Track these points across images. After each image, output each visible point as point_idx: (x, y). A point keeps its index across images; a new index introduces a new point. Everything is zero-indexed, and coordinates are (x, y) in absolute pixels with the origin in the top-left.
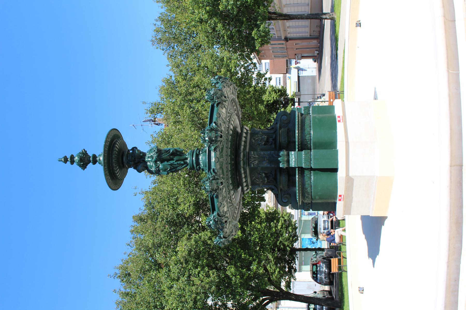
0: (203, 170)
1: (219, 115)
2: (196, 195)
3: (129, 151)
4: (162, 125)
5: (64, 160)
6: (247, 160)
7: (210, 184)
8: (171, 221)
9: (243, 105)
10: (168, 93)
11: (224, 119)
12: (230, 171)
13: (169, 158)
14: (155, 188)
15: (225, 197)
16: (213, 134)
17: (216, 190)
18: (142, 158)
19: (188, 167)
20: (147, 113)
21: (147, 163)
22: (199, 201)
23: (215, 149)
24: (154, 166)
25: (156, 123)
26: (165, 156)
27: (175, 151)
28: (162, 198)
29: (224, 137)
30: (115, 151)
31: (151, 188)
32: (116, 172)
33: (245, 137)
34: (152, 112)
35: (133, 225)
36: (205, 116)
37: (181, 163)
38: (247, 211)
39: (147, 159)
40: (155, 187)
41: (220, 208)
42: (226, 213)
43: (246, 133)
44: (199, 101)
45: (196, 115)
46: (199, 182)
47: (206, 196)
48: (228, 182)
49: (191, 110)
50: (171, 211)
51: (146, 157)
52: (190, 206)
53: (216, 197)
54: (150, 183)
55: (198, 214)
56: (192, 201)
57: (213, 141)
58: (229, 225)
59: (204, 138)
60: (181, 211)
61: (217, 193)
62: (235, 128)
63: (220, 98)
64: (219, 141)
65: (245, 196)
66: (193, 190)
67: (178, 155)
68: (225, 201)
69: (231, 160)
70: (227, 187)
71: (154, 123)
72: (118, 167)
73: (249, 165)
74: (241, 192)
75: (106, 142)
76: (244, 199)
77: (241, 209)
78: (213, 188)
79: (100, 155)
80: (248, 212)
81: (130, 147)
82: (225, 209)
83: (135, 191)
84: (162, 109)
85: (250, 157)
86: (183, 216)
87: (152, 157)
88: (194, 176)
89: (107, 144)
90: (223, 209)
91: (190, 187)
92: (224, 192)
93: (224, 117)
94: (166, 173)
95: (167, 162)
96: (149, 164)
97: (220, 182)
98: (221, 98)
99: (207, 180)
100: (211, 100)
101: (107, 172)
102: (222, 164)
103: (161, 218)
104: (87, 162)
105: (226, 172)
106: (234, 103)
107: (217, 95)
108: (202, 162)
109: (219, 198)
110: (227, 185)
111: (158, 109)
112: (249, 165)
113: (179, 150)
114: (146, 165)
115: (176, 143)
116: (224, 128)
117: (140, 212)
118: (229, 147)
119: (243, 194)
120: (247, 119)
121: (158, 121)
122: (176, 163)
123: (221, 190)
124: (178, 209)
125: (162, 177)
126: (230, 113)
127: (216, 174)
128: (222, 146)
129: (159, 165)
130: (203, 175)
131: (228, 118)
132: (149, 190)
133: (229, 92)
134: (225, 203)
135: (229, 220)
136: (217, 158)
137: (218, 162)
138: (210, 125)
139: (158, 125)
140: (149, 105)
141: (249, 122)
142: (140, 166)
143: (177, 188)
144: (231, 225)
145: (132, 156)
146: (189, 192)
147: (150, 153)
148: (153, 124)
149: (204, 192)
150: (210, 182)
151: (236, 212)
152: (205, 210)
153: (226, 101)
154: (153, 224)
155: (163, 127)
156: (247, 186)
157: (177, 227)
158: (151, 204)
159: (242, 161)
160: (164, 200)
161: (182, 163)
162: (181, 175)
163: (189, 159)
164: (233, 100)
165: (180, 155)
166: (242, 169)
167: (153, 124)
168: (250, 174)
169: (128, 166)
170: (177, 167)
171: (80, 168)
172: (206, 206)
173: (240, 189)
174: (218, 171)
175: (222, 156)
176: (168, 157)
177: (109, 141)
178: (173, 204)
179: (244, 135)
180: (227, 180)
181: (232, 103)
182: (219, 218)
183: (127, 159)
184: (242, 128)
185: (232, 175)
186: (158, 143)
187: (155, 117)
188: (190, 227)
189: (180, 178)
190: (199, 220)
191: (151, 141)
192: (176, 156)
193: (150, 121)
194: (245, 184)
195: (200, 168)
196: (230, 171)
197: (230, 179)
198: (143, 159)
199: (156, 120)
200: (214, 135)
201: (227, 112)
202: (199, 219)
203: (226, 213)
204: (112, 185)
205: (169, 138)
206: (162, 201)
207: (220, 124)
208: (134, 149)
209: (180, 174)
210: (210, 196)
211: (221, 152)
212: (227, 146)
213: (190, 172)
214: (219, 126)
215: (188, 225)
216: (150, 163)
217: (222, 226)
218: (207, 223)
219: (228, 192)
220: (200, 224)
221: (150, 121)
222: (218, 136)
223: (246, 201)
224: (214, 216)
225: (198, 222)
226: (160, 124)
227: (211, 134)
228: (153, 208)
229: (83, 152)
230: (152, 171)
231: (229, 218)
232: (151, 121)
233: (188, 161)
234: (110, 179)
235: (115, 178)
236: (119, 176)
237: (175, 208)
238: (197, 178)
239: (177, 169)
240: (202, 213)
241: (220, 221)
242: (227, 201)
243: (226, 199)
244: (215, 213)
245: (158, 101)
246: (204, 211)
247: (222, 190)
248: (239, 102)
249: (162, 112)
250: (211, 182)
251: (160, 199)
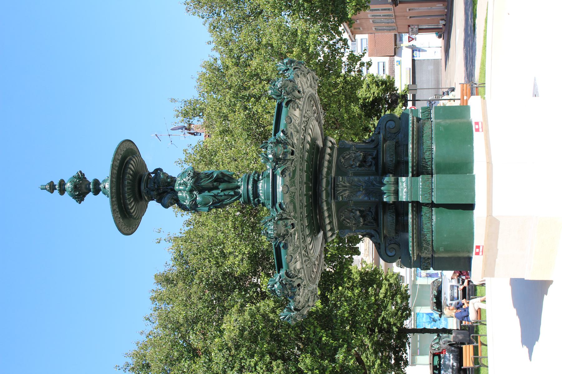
32: (130, 207)
105: (300, 209)
181: (309, 101)
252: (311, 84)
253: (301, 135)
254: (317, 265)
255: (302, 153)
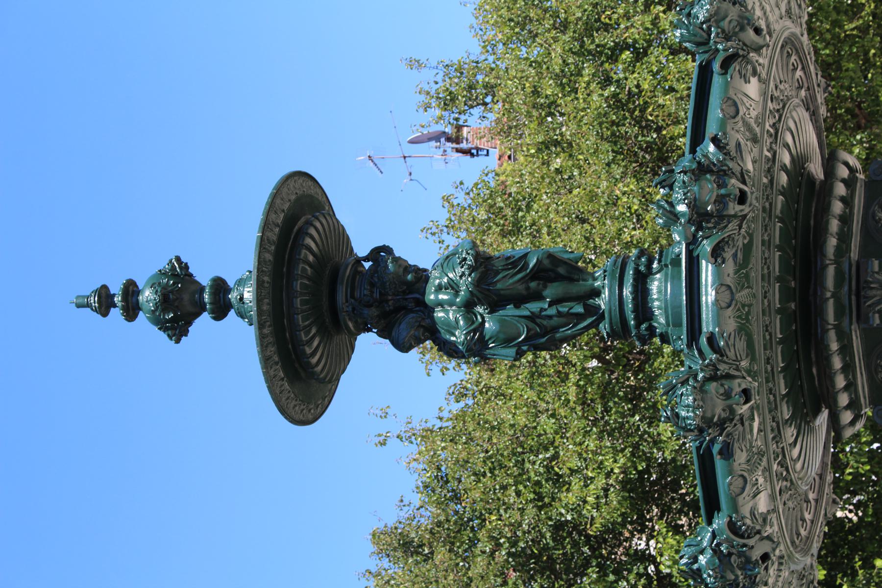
0: (665, 339)
1: (733, 108)
2: (636, 447)
3: (358, 261)
4: (487, 155)
5: (99, 302)
6: (853, 298)
7: (695, 400)
8: (529, 552)
9: (829, 65)
10: (511, 20)
11: (754, 126)
12: (781, 341)
13: (524, 292)
14: (461, 417)
15: (761, 454)
16: (708, 190)
17: (721, 425)
18: (411, 292)
19: (604, 328)
20: (427, 107)
21: (432, 310)
22: (647, 471)
23: (717, 253)
24: (461, 323)
25: (464, 145)
26: (506, 283)
27: (546, 262)
28: (490, 457)
29: (754, 202)
30: (301, 265)
31: (445, 414)
32: (308, 351)
33: (843, 199)
34: (449, 101)
35: (373, 571)
36: (670, 115)
37: (572, 311)
38: (850, 516)
39: (432, 297)
40: (462, 411)
41: (740, 498)
42: (765, 520)
43: (850, 183)
44: (640, 55)
45: (632, 112)
46: (644, 389)
47: (676, 451)
48: (771, 390)
49: (606, 94)
50: (531, 511)
51: (429, 285)
52: (606, 490)
53: (720, 453)
54: (444, 394)
55: (642, 526)
56: (616, 471)
57: (707, 216)
58: (780, 570)
59: (671, 205)
60: (572, 510)
61: (728, 435)
62: (800, 162)
63: (735, 34)
64: (735, 216)
65: (843, 450)
66: (622, 425)
67: (558, 278)
68: (761, 468)
69: (786, 295)
70: (770, 412)
71: (455, 145)
72: (314, 331)
73: (862, 317)
74: (828, 433)
75: (266, 226)
76: (838, 465)
77: (827, 504)
78: (709, 415)
79: (241, 282)
80: (855, 519)
81: (361, 248)
82: (763, 504)
83: (383, 427)
84: (490, 89)
85: (867, 282)
86: (580, 533)
87: (453, 287)
88: (624, 366)
89: (269, 234)
90: (751, 504)
91: (607, 410)
92: (755, 430)
93: (754, 114)
94: (512, 352)
95: (517, 307)
96: (441, 314)
97: (737, 389)
98: (742, 35)
99: (684, 383)
100: (698, 44)
101: (272, 349)
102: (748, 313)
103: (491, 538)
104: (191, 309)
105: (765, 349)
106: (793, 58)
107: (722, 24)
108: (659, 308)
109: (736, 457)
110: (769, 402)
111: (471, 87)
112: (862, 317)
113: (566, 256)
114: (428, 321)
115: (549, 227)
116: (754, 162)
117: (404, 514)
118: (777, 241)
119: (838, 439)
120: (845, 123)
121: (470, 139)
122: (552, 311)
123: (743, 424)
124: (557, 504)
125: (492, 370)
126: (777, 98)
127: (722, 355)
128: (744, 237)
129: (484, 321)
130: (661, 363)
131: (772, 121)
132: (439, 424)
133: (772, 10)
134: (761, 480)
135: (777, 552)
136: (723, 288)
137: (729, 306)
138: (693, 151)
139: (472, 155)
140: (436, 71)
141: (858, 137)
142: (403, 326)
143: (553, 416)
144: (785, 574)
145: (372, 285)
146: (602, 432)
147: (446, 270)
148: (449, 150)
149: (665, 429)
150: (695, 388)
151: (808, 516)
152: (670, 510)
153: (762, 47)
154: (458, 564)
155: (492, 162)
156: (854, 405)
157: (556, 579)
158: (447, 482)
159: (831, 301)
160: (501, 466)
161: (579, 309)
162: (568, 362)
163: (606, 294)
164: (791, 44)
165: (570, 279)
166: (832, 335)
167: (449, 150)
168: (868, 354)
169: (356, 324)
170: (555, 329)
171: (163, 336)
172: (676, 492)
173: (823, 418)
174: (731, 342)
175: (744, 280)
176: (521, 288)
177: (279, 222)
178: (538, 483)
179: (840, 189)
180: (767, 381)
181: (785, 55)
182: (738, 541)
183: (352, 296)
184: (830, 162)
185: (790, 358)
186: (473, 229)
187: (461, 123)
188: (612, 577)
189: (567, 375)
190: (648, 549)
191: (443, 222)
192: (552, 280)
193: (437, 137)
194: (844, 400)
195: (652, 330)
196: (779, 343)
197: (781, 376)
198: (417, 296)
199: (465, 135)
200: (712, 191)
201: (764, 94)
202: (647, 545)
203: (765, 520)
204: (294, 403)
205: (520, 209)
206: (492, 470)
207: (738, 145)
208: (380, 253)
209: (563, 357)
210: (698, 449)
211: (743, 265)
212: (766, 238)
213: (606, 350)
214: (733, 153)
215: (603, 570)
216: (447, 312)
217: (750, 577)
218: (684, 561)
219: (772, 430)
220: (651, 569)
221: (437, 137)
222: (729, 195)
223: (849, 470)
224: (713, 533)
225: (644, 557)
226: (481, 149)
227: (701, 188)
228: (456, 498)
229: (173, 267)
230: (454, 344)
231: (779, 543)
232: (443, 140)
233: (603, 302)
234: (282, 379)
235: (303, 374)
236: (320, 368)
237: (547, 500)
238: (636, 375)
239: (558, 335)
240: (661, 518)
241: (740, 555)
242: (768, 469)
243: (764, 463)
244: (720, 522)
245: (472, 58)
246: (665, 511)
247: (747, 424)
248: (816, 51)
249: (488, 99)
250: (700, 390)
251: (484, 461)
252: (790, 8)
253: (765, 149)
254: (808, 522)
255: (767, 199)
